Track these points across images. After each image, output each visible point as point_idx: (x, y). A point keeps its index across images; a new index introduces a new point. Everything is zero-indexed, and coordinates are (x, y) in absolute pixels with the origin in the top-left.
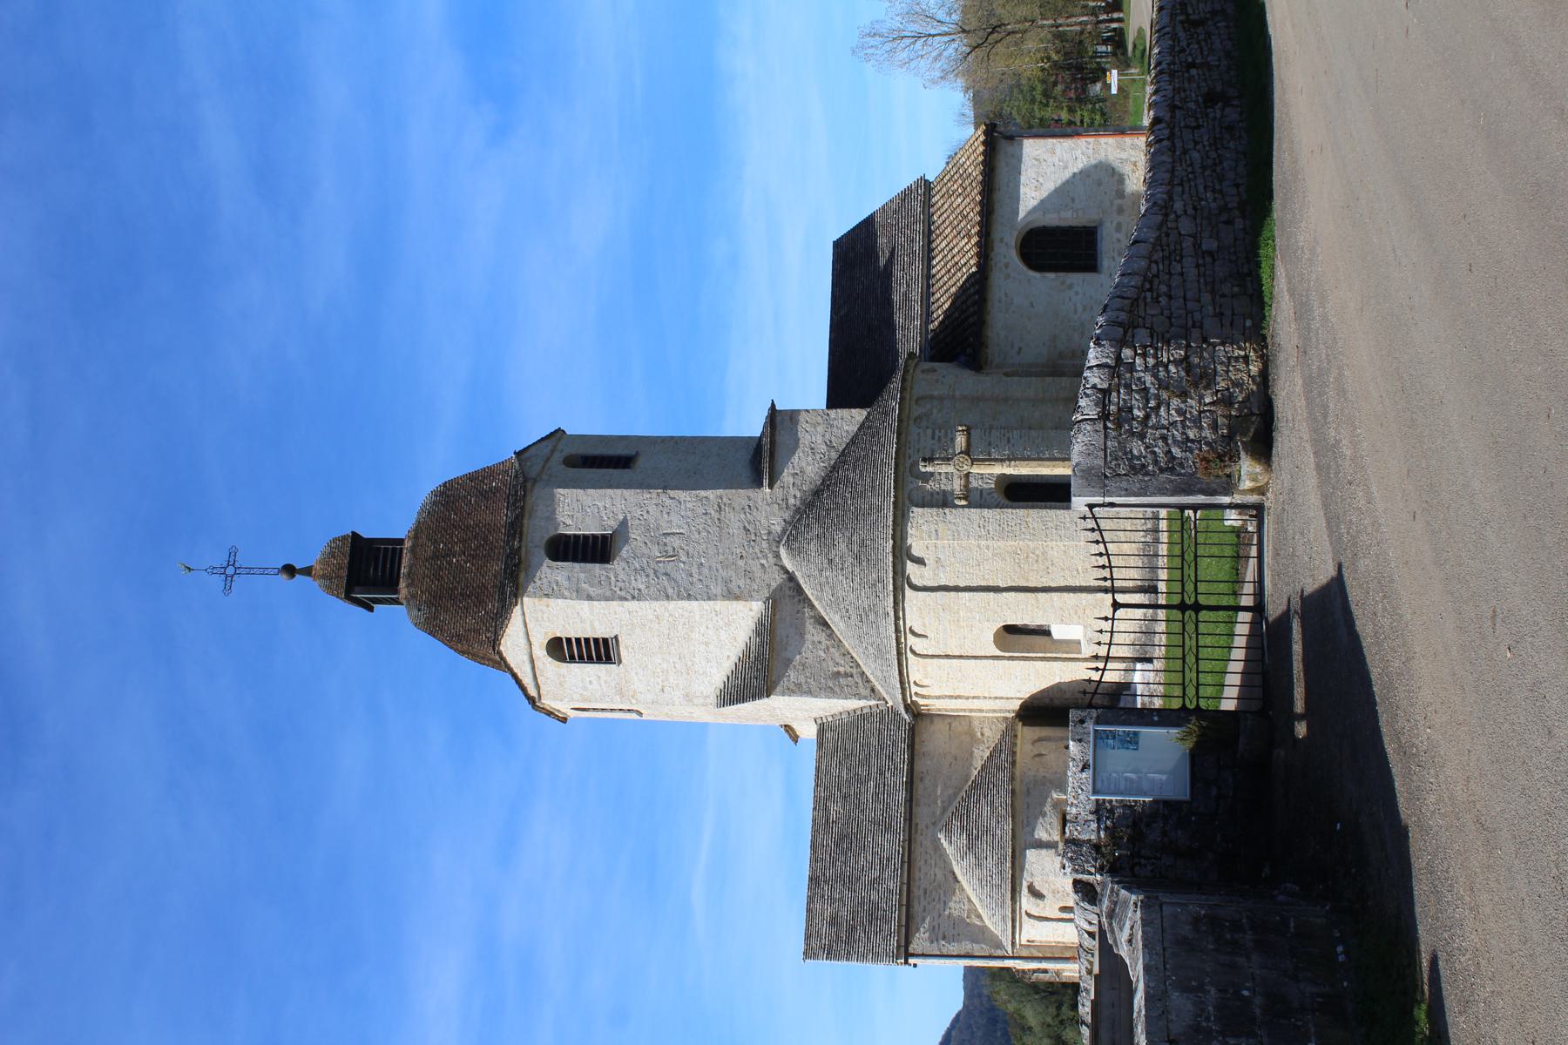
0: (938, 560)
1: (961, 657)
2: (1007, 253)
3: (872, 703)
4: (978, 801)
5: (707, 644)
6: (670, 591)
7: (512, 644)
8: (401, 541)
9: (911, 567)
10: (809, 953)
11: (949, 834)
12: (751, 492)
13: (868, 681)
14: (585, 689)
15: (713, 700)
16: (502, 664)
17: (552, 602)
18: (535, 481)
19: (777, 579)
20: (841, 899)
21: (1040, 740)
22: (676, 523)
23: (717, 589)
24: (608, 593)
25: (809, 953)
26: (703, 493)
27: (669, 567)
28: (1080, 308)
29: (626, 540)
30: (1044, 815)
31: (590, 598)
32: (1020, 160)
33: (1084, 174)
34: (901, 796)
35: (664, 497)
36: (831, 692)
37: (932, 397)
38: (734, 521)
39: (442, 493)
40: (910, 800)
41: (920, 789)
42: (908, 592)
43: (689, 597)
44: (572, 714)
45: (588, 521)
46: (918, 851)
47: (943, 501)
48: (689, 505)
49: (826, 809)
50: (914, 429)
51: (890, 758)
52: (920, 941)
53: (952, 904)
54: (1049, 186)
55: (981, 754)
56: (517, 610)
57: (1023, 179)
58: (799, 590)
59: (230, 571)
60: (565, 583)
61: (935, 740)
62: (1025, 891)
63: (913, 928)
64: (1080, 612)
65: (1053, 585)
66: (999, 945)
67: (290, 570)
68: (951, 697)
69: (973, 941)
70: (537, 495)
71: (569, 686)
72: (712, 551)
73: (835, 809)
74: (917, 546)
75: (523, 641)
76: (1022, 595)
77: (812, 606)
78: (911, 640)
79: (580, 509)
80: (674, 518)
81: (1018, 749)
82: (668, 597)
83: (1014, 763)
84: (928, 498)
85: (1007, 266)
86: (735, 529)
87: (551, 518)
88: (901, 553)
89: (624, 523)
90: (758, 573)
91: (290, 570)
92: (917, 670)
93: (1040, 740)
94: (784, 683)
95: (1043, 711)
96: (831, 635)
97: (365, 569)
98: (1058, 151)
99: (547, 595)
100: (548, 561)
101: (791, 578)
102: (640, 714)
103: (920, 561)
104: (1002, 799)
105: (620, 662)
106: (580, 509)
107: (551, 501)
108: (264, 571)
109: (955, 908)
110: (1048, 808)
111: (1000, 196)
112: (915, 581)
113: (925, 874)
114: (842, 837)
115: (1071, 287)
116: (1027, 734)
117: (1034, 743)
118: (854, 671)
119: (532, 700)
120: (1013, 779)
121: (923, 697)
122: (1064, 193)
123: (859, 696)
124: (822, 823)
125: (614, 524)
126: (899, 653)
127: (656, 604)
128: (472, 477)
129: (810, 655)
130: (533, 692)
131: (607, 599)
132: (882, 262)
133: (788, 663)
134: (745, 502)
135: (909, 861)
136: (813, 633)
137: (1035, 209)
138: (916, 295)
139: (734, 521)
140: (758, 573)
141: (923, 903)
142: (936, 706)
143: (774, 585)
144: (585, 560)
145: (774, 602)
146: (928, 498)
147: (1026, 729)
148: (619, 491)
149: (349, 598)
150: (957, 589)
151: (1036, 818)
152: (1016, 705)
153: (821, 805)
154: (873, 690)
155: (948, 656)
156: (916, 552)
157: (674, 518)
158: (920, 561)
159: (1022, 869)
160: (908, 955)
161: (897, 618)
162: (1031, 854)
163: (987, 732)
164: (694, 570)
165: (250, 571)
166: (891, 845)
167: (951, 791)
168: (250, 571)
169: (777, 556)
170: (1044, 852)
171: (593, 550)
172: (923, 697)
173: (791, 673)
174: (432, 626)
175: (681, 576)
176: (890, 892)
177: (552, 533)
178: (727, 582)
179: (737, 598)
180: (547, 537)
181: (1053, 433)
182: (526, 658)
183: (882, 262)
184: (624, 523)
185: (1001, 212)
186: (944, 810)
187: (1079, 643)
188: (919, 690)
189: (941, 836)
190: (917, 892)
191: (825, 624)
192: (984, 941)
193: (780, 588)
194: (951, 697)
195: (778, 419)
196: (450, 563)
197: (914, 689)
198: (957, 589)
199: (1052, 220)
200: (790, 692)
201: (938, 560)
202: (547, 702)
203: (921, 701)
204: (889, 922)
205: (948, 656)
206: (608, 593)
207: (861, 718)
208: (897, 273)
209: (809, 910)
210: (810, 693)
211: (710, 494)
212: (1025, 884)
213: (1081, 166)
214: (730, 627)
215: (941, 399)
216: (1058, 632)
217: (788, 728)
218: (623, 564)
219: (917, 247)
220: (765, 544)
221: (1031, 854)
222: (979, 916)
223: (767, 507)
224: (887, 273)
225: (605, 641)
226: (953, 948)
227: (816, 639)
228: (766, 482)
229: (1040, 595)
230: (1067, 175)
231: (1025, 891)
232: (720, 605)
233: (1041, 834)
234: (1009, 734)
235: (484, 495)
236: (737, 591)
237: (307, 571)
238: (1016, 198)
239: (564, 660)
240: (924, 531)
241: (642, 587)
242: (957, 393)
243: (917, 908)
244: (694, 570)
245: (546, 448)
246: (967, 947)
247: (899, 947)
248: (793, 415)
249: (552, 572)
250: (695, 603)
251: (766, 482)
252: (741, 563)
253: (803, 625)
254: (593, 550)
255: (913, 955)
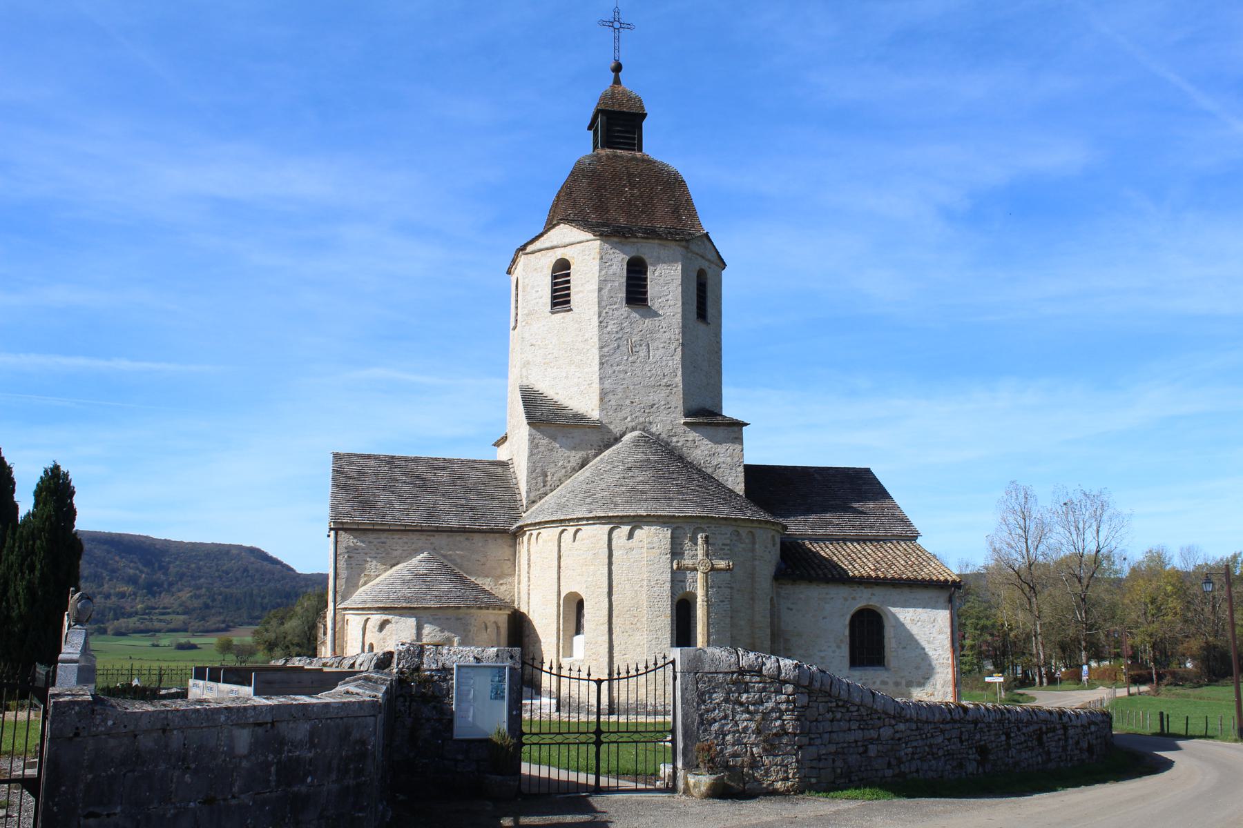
0: (631, 549)
1: (559, 567)
2: (864, 599)
3: (524, 502)
4: (452, 582)
5: (567, 377)
6: (606, 350)
7: (565, 233)
8: (640, 150)
9: (626, 529)
10: (337, 457)
11: (427, 560)
12: (680, 408)
13: (540, 498)
14: (533, 287)
15: (525, 383)
16: (550, 226)
17: (597, 261)
18: (687, 248)
19: (616, 429)
20: (378, 480)
21: (498, 628)
22: (657, 353)
23: (608, 384)
24: (604, 304)
25: (337, 457)
26: (679, 373)
27: (623, 348)
28: (822, 654)
29: (644, 316)
30: (442, 631)
31: (600, 290)
32: (934, 608)
33: (924, 657)
34: (455, 524)
35: (676, 343)
36: (532, 471)
37: (754, 543)
38: (659, 396)
39: (676, 179)
40: (451, 531)
41: (459, 538)
42: (608, 527)
43: (602, 364)
44: (513, 278)
45: (657, 288)
46: (415, 536)
47: (676, 552)
48: (670, 363)
49: (445, 468)
50: (730, 529)
51: (483, 516)
52: (347, 539)
53: (374, 563)
54: (914, 630)
55: (486, 583)
56: (590, 236)
57: (920, 610)
58: (608, 446)
59: (617, 25)
60: (611, 272)
61: (496, 550)
62: (385, 617)
63: (357, 534)
64: (594, 657)
65: (614, 636)
66: (344, 599)
67: (618, 68)
68: (529, 560)
69: (347, 579)
70: (675, 249)
71: (534, 275)
72: (636, 380)
73: (445, 474)
74: (643, 533)
75: (567, 241)
76: (606, 612)
77: (596, 456)
78: (571, 530)
79: (667, 282)
80: (660, 352)
81: (490, 611)
82: (601, 348)
83: (480, 608)
84: (678, 541)
85: (854, 599)
86: (653, 397)
87: (659, 260)
88: (636, 522)
89: (656, 314)
90: (621, 415)
91: (618, 68)
92: (550, 534)
93: (498, 628)
94: (539, 435)
95: (519, 630)
96: (575, 470)
97: (619, 124)
98: (941, 636)
99: (601, 258)
100: (627, 258)
101: (617, 440)
102: (514, 329)
103: (630, 536)
104: (453, 599)
105: (553, 313)
106: (667, 282)
107: (672, 261)
108: (617, 49)
109: (372, 565)
110: (447, 634)
111: (906, 593)
112: (616, 532)
113: (397, 542)
114: (424, 481)
115: (839, 647)
116: (502, 617)
117: (496, 623)
118: (548, 488)
119: (523, 248)
120: (469, 607)
121: (529, 540)
122: (909, 641)
123: (529, 491)
124: (434, 465)
125: (655, 307)
126: (561, 521)
127: (596, 339)
128: (689, 201)
129: (559, 454)
130: (530, 249)
131: (599, 303)
132: (855, 505)
133: (553, 438)
134: (673, 404)
135: (406, 530)
136: (576, 457)
137: (897, 619)
138: (830, 530)
139: (659, 396)
140: (621, 415)
141: (375, 542)
142: (523, 550)
143: (611, 427)
144: (628, 286)
145: (599, 427)
146: (678, 541)
147: (506, 617)
148: (680, 310)
149: (598, 112)
150: (610, 564)
151: (439, 625)
152: (524, 609)
153: (448, 464)
154: (534, 502)
155: (559, 557)
156: (637, 532)
157: (660, 352)
158: (630, 536)
159: (401, 615)
160: (336, 530)
161: (588, 519)
162: (412, 622)
163: (503, 588)
164: (621, 368)
165: (617, 39)
166: (419, 516)
167: (459, 561)
168: (617, 39)
169: (633, 429)
170: (414, 631)
171: (636, 293)
172: (529, 540)
173: (546, 441)
174: (578, 174)
175: (617, 357)
176: (383, 517)
177: (648, 261)
178: (613, 392)
179: (601, 400)
180: (645, 257)
181: (728, 634)
182: (555, 243)
183: (855, 505)
184: (656, 314)
185: (894, 594)
186: (444, 556)
187: (571, 656)
188: (534, 537)
189: (425, 554)
190: (383, 537)
191: (582, 466)
192: (347, 587)
193: (610, 432)
194: (529, 560)
195: (736, 429)
196: (625, 186)
197: (535, 533)
198: (610, 564)
199: (889, 633)
200: (532, 440)
201: (631, 549)
202: (522, 260)
203: (526, 538)
204: (361, 516)
205: (559, 557)
206: (604, 304)
207: (513, 493)
208: (847, 516)
209: (369, 456)
210: (531, 454)
211: (679, 378)
212: (390, 617)
213: (930, 653)
214: (580, 395)
215: (753, 550)
216: (578, 640)
217: (504, 439)
218: (625, 314)
219: (867, 531)
220: (642, 420)
221: (412, 622)
222: (365, 583)
223: (670, 421)
224: (846, 509)
225: (568, 302)
226: (342, 564)
227: (572, 459)
228: (688, 420)
229: (606, 627)
230: (923, 643)
231: (385, 617)
232: (596, 386)
233: (428, 629)
234: (502, 604)
235: (675, 210)
236: (607, 399)
237: (617, 81)
238: (905, 605)
239: (554, 271)
240: (653, 539)
241: (609, 329)
242: (757, 563)
243: (372, 536)
244: (621, 368)
245: (713, 257)
246: (343, 574)
247: (342, 523)
248: (739, 439)
249: (619, 262)
250: (597, 368)
251: (688, 420)
252: (628, 402)
253: (582, 449)
254: (636, 293)
255: (336, 534)
